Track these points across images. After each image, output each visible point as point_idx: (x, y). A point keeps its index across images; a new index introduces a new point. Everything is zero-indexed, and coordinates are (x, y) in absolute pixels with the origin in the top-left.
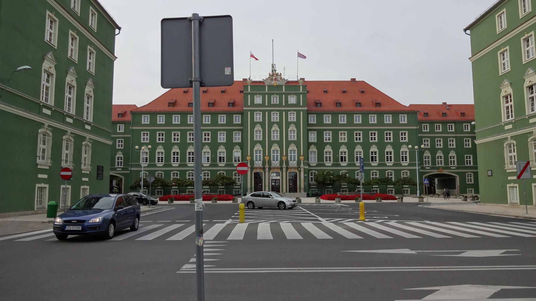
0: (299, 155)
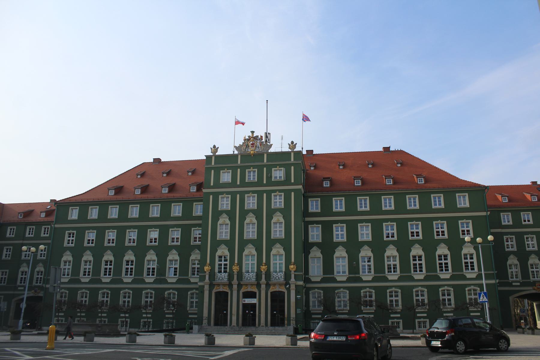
0: (288, 262)
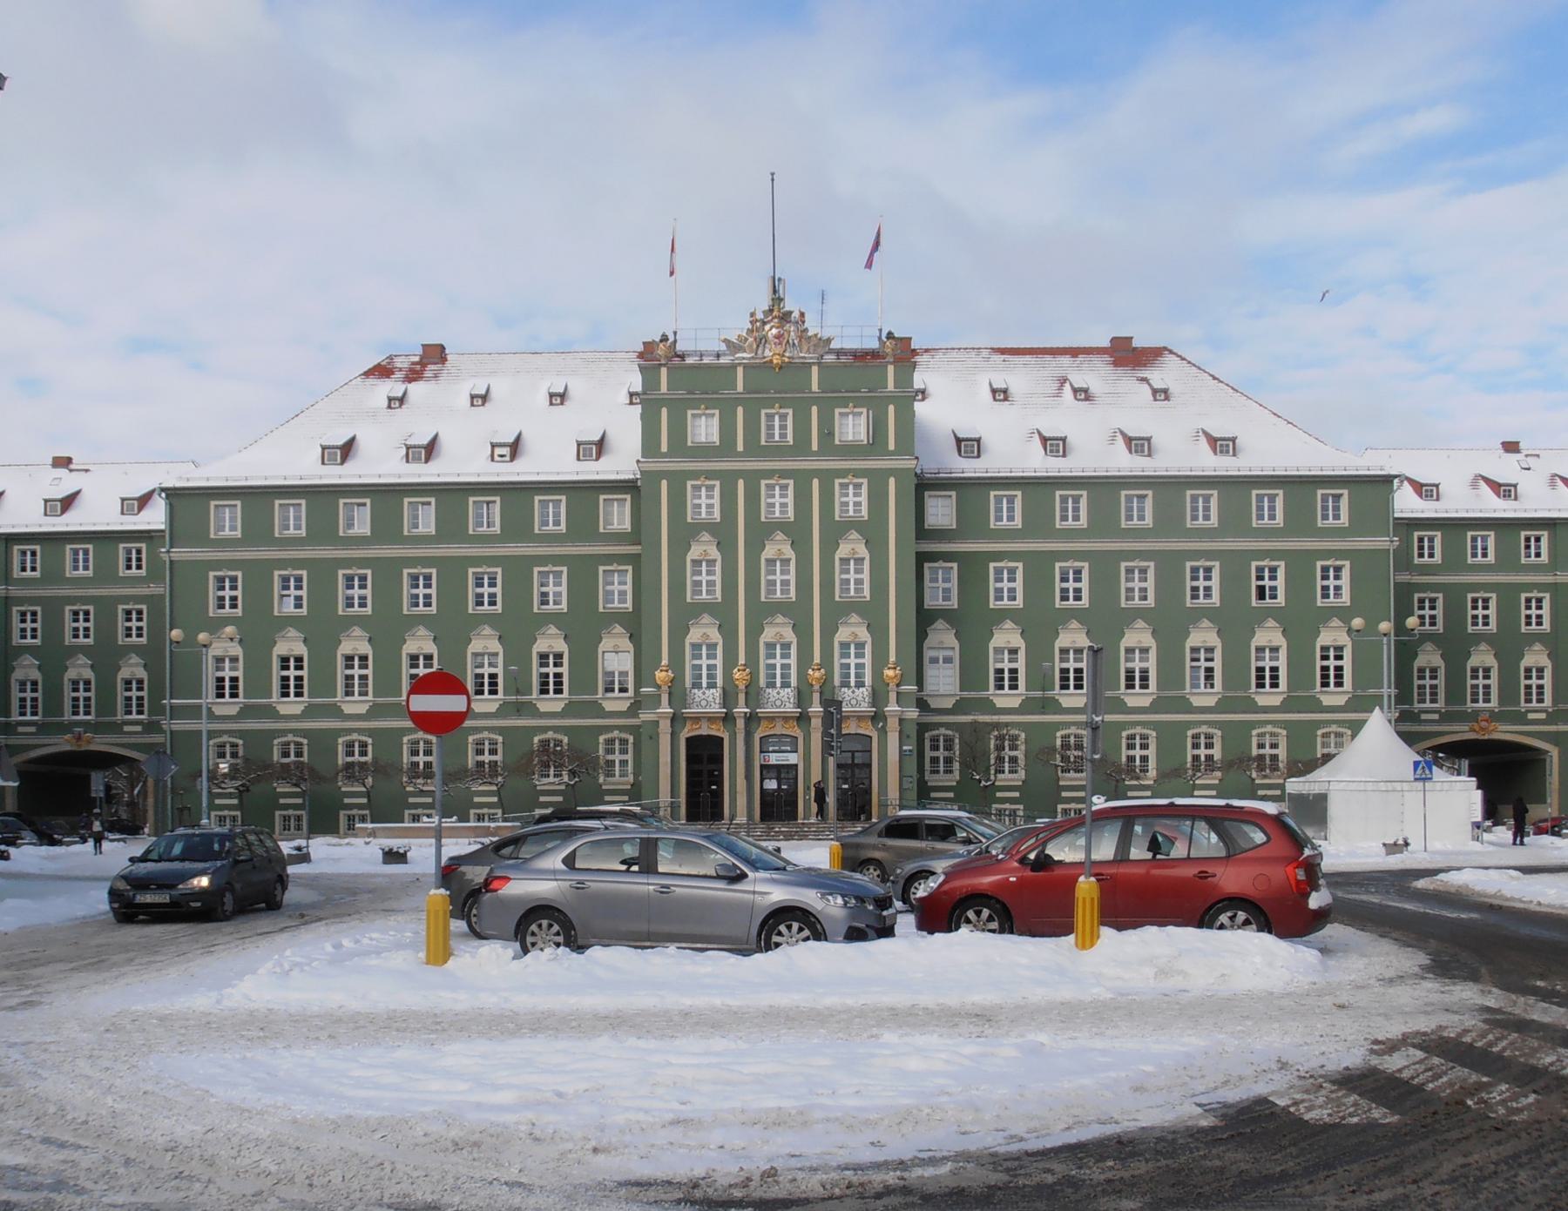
0: (880, 661)
